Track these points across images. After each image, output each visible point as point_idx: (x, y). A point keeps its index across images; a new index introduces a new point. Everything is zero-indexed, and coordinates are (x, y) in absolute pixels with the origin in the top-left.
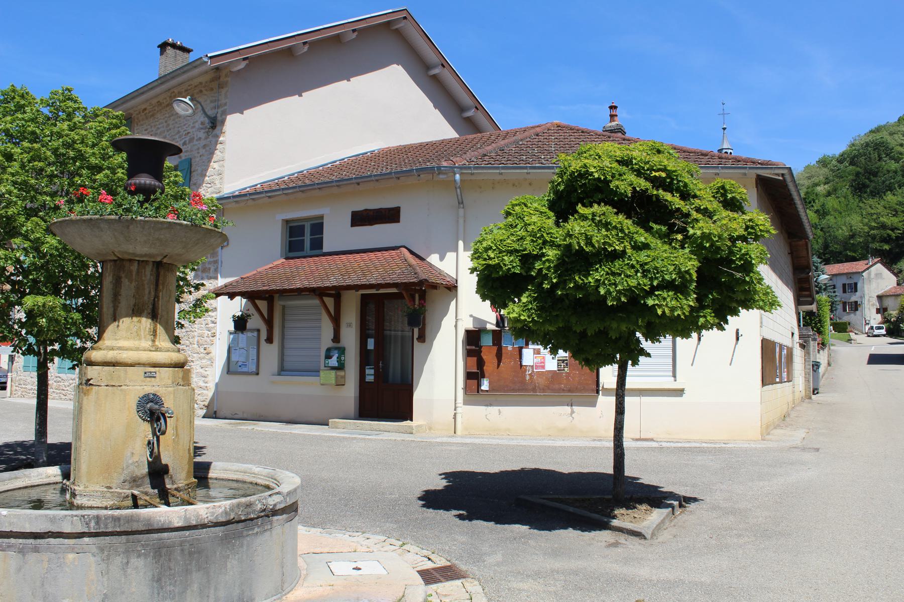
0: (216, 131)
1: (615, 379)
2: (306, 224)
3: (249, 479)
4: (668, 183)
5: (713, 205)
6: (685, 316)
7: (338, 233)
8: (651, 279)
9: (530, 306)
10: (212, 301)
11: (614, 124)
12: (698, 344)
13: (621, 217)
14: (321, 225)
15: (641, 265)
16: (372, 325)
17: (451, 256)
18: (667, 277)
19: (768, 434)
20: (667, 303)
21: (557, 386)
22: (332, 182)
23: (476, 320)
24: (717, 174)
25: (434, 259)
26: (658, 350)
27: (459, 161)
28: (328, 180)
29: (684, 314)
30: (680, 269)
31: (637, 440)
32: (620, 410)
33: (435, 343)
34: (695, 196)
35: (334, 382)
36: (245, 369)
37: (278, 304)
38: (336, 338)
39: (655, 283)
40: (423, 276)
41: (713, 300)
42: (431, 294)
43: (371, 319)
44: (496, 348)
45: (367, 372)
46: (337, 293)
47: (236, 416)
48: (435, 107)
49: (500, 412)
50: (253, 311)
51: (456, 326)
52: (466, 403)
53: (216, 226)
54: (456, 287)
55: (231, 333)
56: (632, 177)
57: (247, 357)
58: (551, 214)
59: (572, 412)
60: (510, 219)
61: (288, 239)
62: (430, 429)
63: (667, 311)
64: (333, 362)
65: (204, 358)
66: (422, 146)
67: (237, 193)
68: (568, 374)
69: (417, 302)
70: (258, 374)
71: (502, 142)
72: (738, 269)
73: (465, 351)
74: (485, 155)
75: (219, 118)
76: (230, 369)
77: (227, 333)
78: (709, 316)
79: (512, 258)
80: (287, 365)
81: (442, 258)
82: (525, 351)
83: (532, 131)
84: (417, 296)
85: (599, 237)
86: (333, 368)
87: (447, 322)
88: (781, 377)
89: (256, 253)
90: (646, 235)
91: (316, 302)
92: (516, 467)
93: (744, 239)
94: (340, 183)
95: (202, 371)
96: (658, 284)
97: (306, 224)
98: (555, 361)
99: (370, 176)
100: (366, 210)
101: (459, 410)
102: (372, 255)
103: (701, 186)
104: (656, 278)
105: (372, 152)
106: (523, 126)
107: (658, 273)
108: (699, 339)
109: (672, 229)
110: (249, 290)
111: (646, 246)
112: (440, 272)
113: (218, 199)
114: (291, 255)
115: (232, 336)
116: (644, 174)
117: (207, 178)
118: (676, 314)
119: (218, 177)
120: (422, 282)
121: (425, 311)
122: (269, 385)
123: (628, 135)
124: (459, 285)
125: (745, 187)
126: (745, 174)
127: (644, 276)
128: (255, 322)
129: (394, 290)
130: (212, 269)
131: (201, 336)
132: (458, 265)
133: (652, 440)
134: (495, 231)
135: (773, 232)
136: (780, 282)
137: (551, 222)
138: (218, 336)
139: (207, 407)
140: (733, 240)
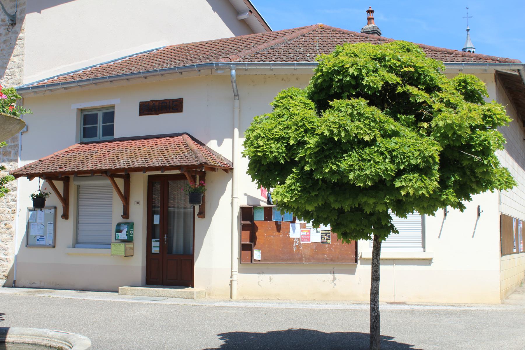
0: (16, 28)
1: (371, 250)
2: (98, 112)
3: (44, 342)
4: (413, 78)
5: (457, 98)
6: (430, 195)
8: (399, 164)
9: (293, 187)
10: (12, 182)
11: (371, 26)
12: (444, 219)
13: (373, 108)
14: (113, 114)
15: (390, 153)
16: (158, 203)
17: (227, 142)
18: (413, 162)
19: (507, 298)
20: (411, 184)
21: (320, 256)
22: (122, 76)
23: (249, 198)
24: (461, 70)
25: (212, 144)
26: (407, 224)
27: (235, 59)
28: (118, 74)
29: (428, 192)
30: (424, 154)
31: (391, 303)
32: (376, 277)
33: (214, 218)
34: (439, 89)
35: (123, 253)
37: (74, 184)
38: (126, 214)
39: (402, 167)
40: (203, 160)
41: (455, 181)
42: (210, 175)
43: (157, 197)
45: (154, 244)
46: (126, 174)
47: (34, 285)
48: (214, 10)
49: (271, 279)
50: (50, 190)
51: (232, 204)
52: (241, 271)
53: (14, 114)
54: (232, 169)
56: (383, 72)
58: (313, 105)
59: (334, 279)
60: (278, 110)
61: (83, 126)
62: (209, 294)
63: (411, 191)
64: (123, 235)
65: (5, 233)
66: (202, 45)
67: (35, 85)
69: (198, 182)
70: (54, 247)
71: (273, 42)
72: (477, 153)
73: (240, 226)
74: (258, 53)
75: (18, 16)
76: (29, 242)
77: (26, 211)
78: (450, 195)
79: (279, 145)
80: (81, 239)
81: (220, 144)
83: (300, 32)
84: (198, 177)
85: (353, 127)
86: (123, 241)
87: (225, 200)
88: (518, 248)
89: (55, 139)
90: (395, 124)
91: (108, 182)
92: (283, 328)
93: (483, 128)
94: (129, 77)
96: (404, 169)
97: (98, 112)
98: (319, 235)
99: (156, 71)
100: (152, 101)
101: (235, 278)
102: (158, 141)
103: (445, 80)
104: (403, 163)
105: (158, 50)
106: (291, 27)
107: (404, 158)
108: (445, 215)
109: (419, 118)
110: (47, 171)
111: (395, 134)
112: (218, 156)
113: (18, 90)
114: (85, 140)
115: (30, 213)
116: (395, 70)
117: (7, 70)
118: (420, 193)
119: (17, 70)
120: (201, 165)
121: (205, 190)
122: (65, 256)
123: (383, 36)
124: (235, 167)
125: (485, 81)
126: (486, 70)
127: (392, 162)
128: (52, 200)
129: (177, 172)
130: (13, 152)
132: (232, 150)
133: (404, 303)
134: (266, 122)
135: (509, 120)
136: (516, 165)
137: (312, 113)
138: (18, 213)
140: (473, 129)
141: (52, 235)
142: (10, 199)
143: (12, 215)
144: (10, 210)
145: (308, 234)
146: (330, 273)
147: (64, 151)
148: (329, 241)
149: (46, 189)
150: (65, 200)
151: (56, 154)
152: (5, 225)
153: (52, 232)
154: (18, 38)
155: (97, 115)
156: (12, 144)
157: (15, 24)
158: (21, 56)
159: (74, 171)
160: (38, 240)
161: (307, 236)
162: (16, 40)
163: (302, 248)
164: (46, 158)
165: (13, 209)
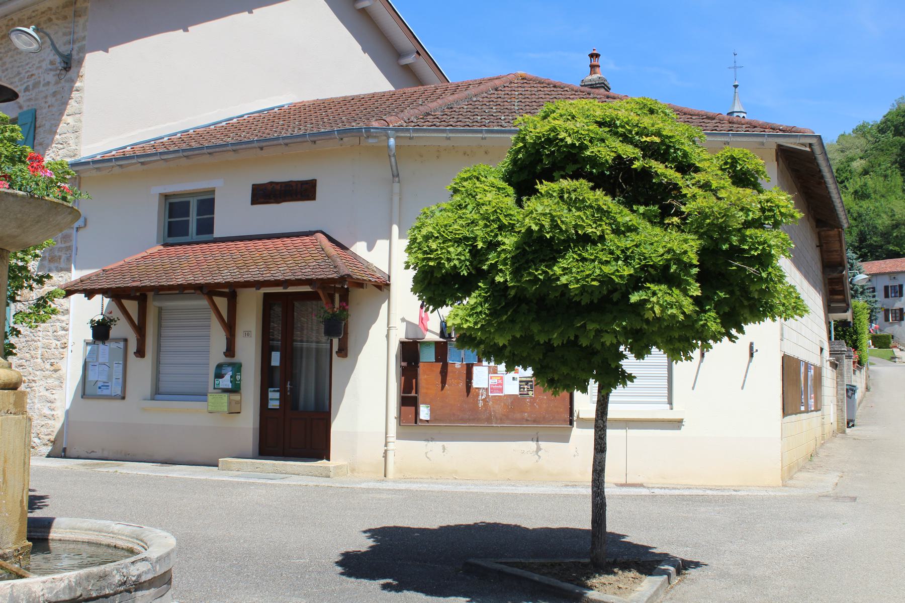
0: (71, 74)
2: (191, 199)
7: (234, 213)
14: (212, 201)
21: (518, 416)
35: (226, 409)
36: (106, 392)
38: (230, 351)
50: (117, 313)
52: (400, 436)
55: (87, 344)
57: (110, 377)
61: (167, 220)
62: (353, 470)
64: (226, 382)
65: (50, 377)
68: (533, 400)
70: (123, 398)
76: (85, 391)
77: (83, 344)
80: (163, 387)
82: (476, 370)
95: (47, 394)
97: (191, 199)
98: (517, 383)
100: (271, 183)
101: (391, 446)
114: (171, 240)
115: (89, 348)
119: (72, 135)
128: (121, 329)
130: (64, 257)
138: (70, 348)
139: (54, 442)
141: (120, 381)
144: (58, 343)
147: (139, 256)
151: (127, 260)
153: (120, 376)
155: (188, 202)
156: (63, 245)
161: (498, 384)
163: (490, 403)
165: (63, 341)
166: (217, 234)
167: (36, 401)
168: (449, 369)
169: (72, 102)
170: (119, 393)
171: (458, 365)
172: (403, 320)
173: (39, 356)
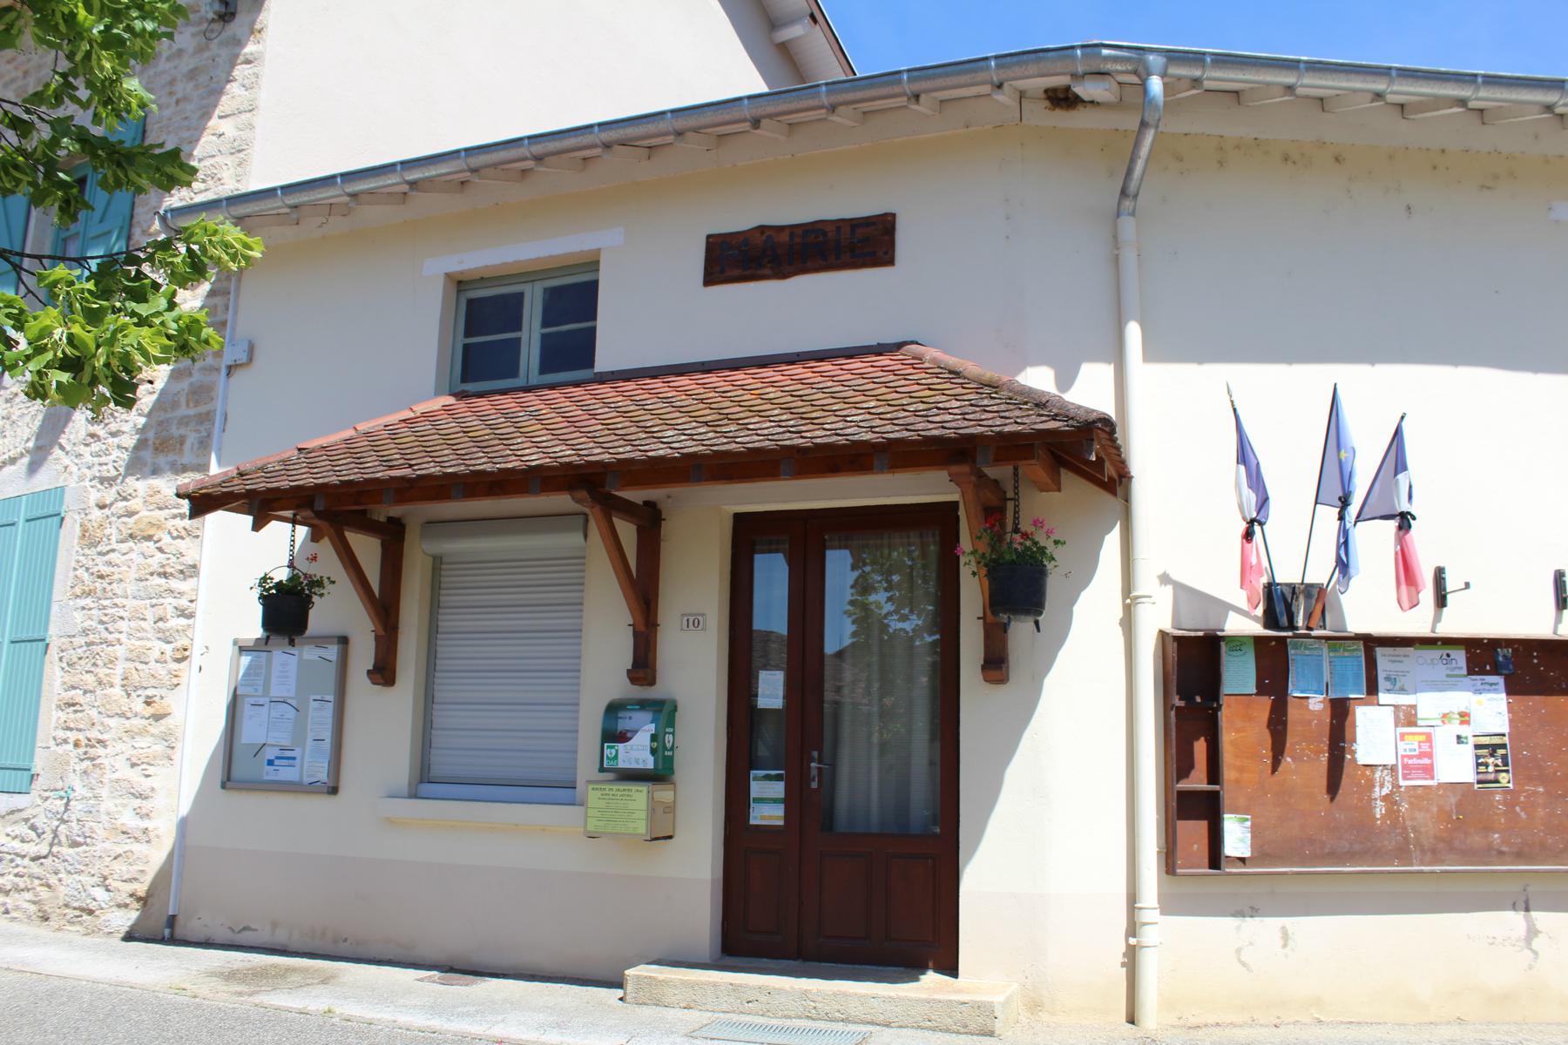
0: (235, 27)
2: (527, 289)
7: (656, 308)
14: (592, 287)
21: (1476, 840)
33: (1052, 682)
35: (641, 828)
36: (287, 774)
38: (643, 667)
44: (1266, 702)
45: (757, 788)
50: (329, 564)
52: (1169, 906)
55: (243, 650)
57: (299, 733)
59: (1532, 932)
61: (461, 340)
62: (1035, 1006)
64: (637, 752)
65: (143, 732)
68: (1511, 797)
70: (334, 790)
76: (234, 770)
77: (229, 650)
80: (442, 763)
95: (134, 775)
97: (527, 289)
98: (1468, 751)
100: (762, 229)
101: (1149, 936)
114: (470, 387)
115: (245, 660)
119: (229, 160)
122: (376, 831)
128: (338, 608)
130: (192, 439)
131: (139, 658)
138: (196, 659)
139: (144, 901)
141: (327, 745)
142: (170, 610)
143: (175, 666)
144: (168, 648)
145: (1425, 748)
146: (1514, 908)
147: (394, 418)
148: (1504, 778)
149: (315, 558)
150: (385, 610)
151: (363, 427)
152: (148, 703)
153: (327, 735)
154: (241, 58)
155: (519, 297)
156: (192, 412)
157: (233, 15)
158: (245, 116)
159: (454, 474)
160: (270, 763)
161: (1421, 755)
162: (233, 65)
163: (1404, 807)
164: (324, 442)
165: (179, 644)
166: (603, 363)
167: (104, 792)
168: (1293, 713)
169: (233, 88)
170: (323, 775)
171: (1317, 703)
172: (1165, 579)
173: (117, 681)
